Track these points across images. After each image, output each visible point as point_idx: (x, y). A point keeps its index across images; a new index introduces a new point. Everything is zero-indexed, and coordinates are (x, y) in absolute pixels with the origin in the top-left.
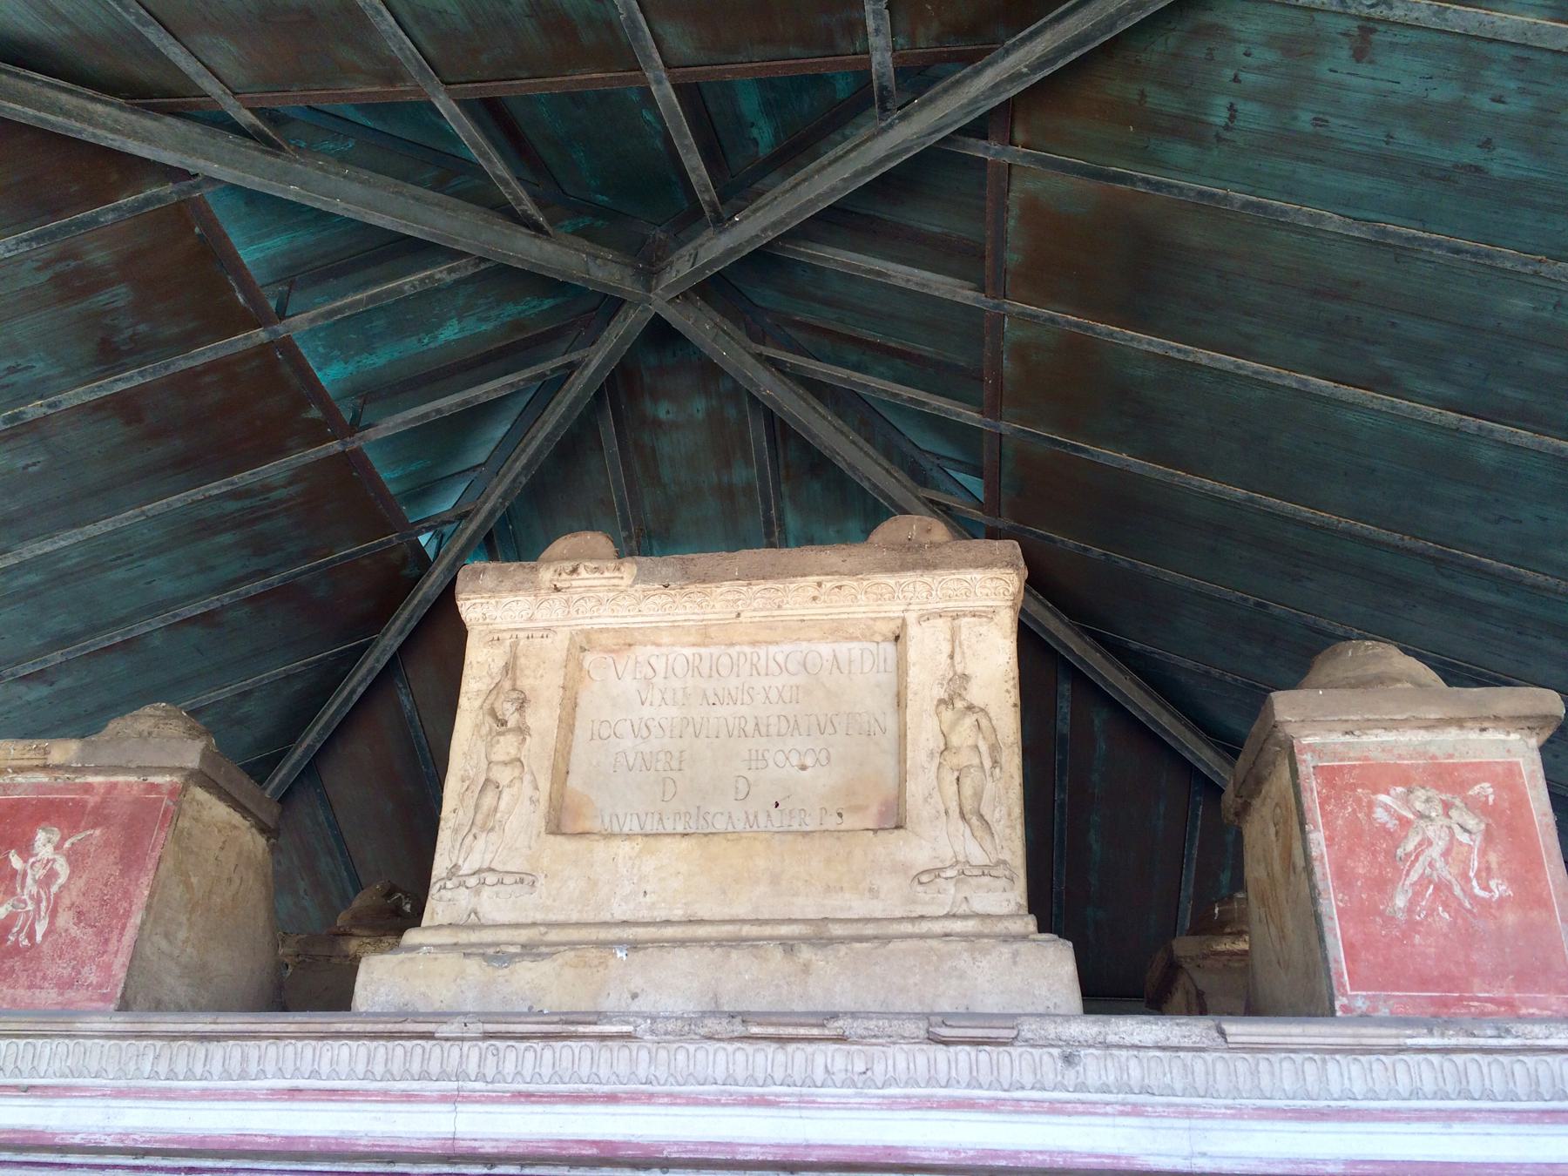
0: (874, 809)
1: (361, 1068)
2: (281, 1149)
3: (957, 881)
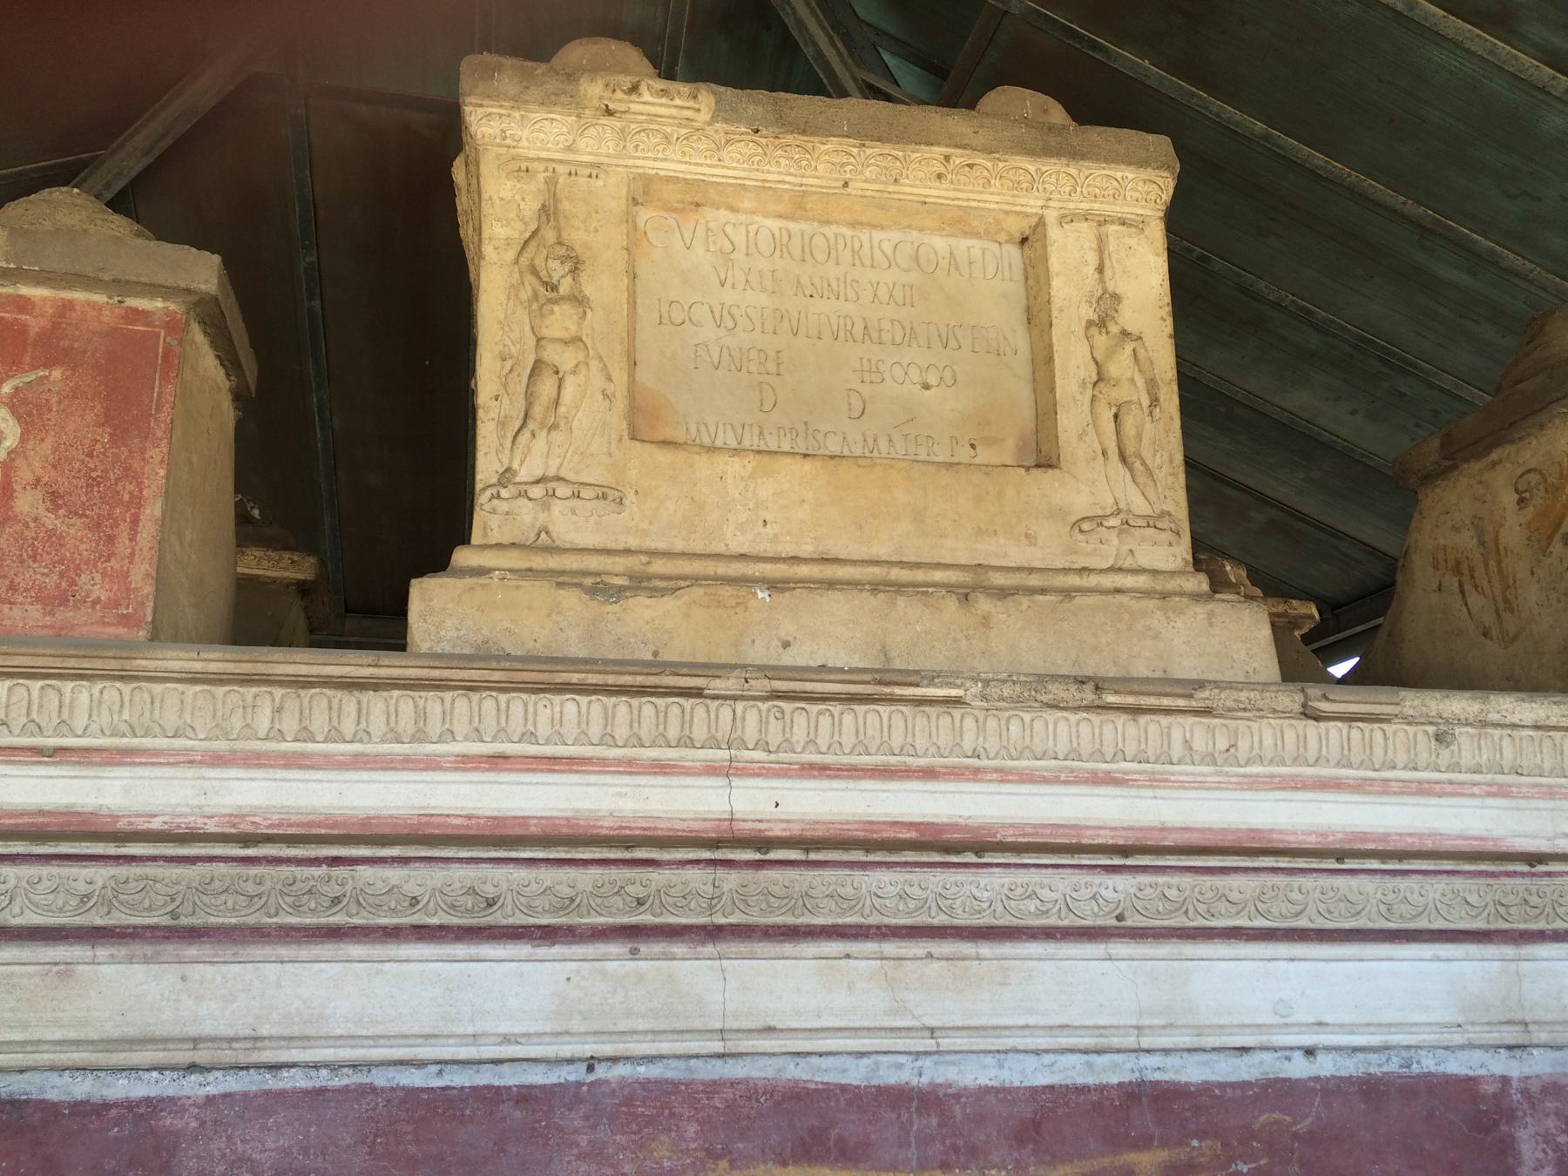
0: (1011, 443)
1: (595, 730)
2: (487, 833)
3: (1121, 532)
